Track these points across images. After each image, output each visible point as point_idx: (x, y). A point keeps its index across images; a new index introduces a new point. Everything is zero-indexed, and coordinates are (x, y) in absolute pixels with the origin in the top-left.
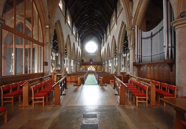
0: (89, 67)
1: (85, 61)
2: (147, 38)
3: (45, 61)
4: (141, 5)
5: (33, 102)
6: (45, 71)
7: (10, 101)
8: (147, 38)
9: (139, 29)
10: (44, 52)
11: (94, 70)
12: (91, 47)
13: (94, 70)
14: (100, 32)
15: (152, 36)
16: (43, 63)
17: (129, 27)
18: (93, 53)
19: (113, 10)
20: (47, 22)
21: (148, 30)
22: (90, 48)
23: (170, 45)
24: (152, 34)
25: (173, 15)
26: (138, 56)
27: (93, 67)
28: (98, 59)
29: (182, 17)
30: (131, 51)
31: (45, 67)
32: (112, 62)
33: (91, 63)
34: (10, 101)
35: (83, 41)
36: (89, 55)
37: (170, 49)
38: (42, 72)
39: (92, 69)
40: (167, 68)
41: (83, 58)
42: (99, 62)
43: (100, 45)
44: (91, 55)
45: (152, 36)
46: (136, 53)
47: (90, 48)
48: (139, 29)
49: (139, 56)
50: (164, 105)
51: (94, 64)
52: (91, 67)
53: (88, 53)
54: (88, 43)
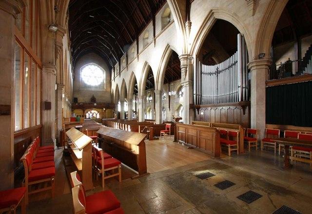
0: (89, 112)
1: (81, 100)
2: (210, 74)
3: (44, 100)
4: (202, 30)
5: (104, 178)
6: (45, 120)
7: (273, 143)
8: (210, 74)
9: (198, 60)
10: (44, 81)
11: (98, 117)
12: (92, 75)
13: (98, 117)
14: (113, 51)
15: (218, 72)
16: (41, 103)
17: (185, 55)
18: (96, 87)
19: (148, 22)
20: (52, 20)
21: (211, 63)
22: (90, 77)
23: (244, 86)
24: (217, 69)
25: (248, 56)
26: (195, 95)
27: (96, 112)
28: (107, 98)
29: (260, 58)
30: (185, 90)
31: (45, 112)
32: (130, 104)
33: (95, 104)
34: (273, 143)
35: (78, 60)
36: (90, 89)
37: (244, 89)
38: (38, 123)
39: (95, 115)
40: (238, 111)
41: (77, 96)
42: (109, 104)
43: (109, 75)
44: (93, 89)
45: (218, 72)
46: (195, 93)
47: (95, 77)
48: (198, 60)
49: (199, 95)
50: (119, 181)
51: (99, 107)
52: (93, 111)
53: (85, 86)
54: (87, 67)
